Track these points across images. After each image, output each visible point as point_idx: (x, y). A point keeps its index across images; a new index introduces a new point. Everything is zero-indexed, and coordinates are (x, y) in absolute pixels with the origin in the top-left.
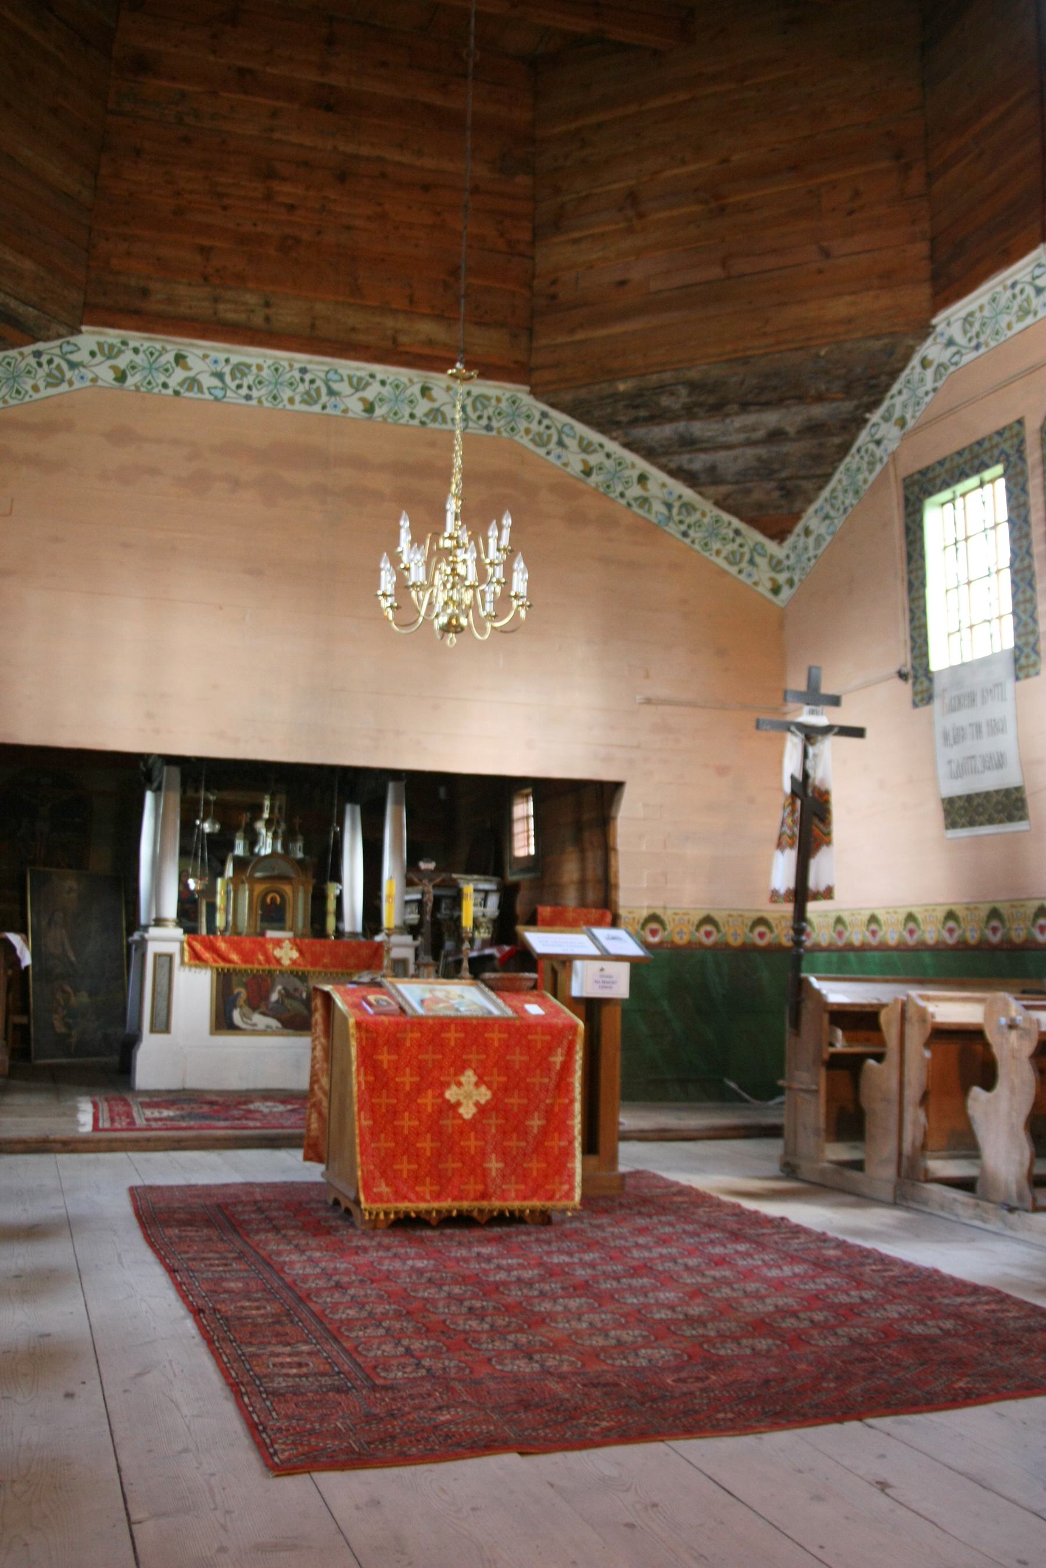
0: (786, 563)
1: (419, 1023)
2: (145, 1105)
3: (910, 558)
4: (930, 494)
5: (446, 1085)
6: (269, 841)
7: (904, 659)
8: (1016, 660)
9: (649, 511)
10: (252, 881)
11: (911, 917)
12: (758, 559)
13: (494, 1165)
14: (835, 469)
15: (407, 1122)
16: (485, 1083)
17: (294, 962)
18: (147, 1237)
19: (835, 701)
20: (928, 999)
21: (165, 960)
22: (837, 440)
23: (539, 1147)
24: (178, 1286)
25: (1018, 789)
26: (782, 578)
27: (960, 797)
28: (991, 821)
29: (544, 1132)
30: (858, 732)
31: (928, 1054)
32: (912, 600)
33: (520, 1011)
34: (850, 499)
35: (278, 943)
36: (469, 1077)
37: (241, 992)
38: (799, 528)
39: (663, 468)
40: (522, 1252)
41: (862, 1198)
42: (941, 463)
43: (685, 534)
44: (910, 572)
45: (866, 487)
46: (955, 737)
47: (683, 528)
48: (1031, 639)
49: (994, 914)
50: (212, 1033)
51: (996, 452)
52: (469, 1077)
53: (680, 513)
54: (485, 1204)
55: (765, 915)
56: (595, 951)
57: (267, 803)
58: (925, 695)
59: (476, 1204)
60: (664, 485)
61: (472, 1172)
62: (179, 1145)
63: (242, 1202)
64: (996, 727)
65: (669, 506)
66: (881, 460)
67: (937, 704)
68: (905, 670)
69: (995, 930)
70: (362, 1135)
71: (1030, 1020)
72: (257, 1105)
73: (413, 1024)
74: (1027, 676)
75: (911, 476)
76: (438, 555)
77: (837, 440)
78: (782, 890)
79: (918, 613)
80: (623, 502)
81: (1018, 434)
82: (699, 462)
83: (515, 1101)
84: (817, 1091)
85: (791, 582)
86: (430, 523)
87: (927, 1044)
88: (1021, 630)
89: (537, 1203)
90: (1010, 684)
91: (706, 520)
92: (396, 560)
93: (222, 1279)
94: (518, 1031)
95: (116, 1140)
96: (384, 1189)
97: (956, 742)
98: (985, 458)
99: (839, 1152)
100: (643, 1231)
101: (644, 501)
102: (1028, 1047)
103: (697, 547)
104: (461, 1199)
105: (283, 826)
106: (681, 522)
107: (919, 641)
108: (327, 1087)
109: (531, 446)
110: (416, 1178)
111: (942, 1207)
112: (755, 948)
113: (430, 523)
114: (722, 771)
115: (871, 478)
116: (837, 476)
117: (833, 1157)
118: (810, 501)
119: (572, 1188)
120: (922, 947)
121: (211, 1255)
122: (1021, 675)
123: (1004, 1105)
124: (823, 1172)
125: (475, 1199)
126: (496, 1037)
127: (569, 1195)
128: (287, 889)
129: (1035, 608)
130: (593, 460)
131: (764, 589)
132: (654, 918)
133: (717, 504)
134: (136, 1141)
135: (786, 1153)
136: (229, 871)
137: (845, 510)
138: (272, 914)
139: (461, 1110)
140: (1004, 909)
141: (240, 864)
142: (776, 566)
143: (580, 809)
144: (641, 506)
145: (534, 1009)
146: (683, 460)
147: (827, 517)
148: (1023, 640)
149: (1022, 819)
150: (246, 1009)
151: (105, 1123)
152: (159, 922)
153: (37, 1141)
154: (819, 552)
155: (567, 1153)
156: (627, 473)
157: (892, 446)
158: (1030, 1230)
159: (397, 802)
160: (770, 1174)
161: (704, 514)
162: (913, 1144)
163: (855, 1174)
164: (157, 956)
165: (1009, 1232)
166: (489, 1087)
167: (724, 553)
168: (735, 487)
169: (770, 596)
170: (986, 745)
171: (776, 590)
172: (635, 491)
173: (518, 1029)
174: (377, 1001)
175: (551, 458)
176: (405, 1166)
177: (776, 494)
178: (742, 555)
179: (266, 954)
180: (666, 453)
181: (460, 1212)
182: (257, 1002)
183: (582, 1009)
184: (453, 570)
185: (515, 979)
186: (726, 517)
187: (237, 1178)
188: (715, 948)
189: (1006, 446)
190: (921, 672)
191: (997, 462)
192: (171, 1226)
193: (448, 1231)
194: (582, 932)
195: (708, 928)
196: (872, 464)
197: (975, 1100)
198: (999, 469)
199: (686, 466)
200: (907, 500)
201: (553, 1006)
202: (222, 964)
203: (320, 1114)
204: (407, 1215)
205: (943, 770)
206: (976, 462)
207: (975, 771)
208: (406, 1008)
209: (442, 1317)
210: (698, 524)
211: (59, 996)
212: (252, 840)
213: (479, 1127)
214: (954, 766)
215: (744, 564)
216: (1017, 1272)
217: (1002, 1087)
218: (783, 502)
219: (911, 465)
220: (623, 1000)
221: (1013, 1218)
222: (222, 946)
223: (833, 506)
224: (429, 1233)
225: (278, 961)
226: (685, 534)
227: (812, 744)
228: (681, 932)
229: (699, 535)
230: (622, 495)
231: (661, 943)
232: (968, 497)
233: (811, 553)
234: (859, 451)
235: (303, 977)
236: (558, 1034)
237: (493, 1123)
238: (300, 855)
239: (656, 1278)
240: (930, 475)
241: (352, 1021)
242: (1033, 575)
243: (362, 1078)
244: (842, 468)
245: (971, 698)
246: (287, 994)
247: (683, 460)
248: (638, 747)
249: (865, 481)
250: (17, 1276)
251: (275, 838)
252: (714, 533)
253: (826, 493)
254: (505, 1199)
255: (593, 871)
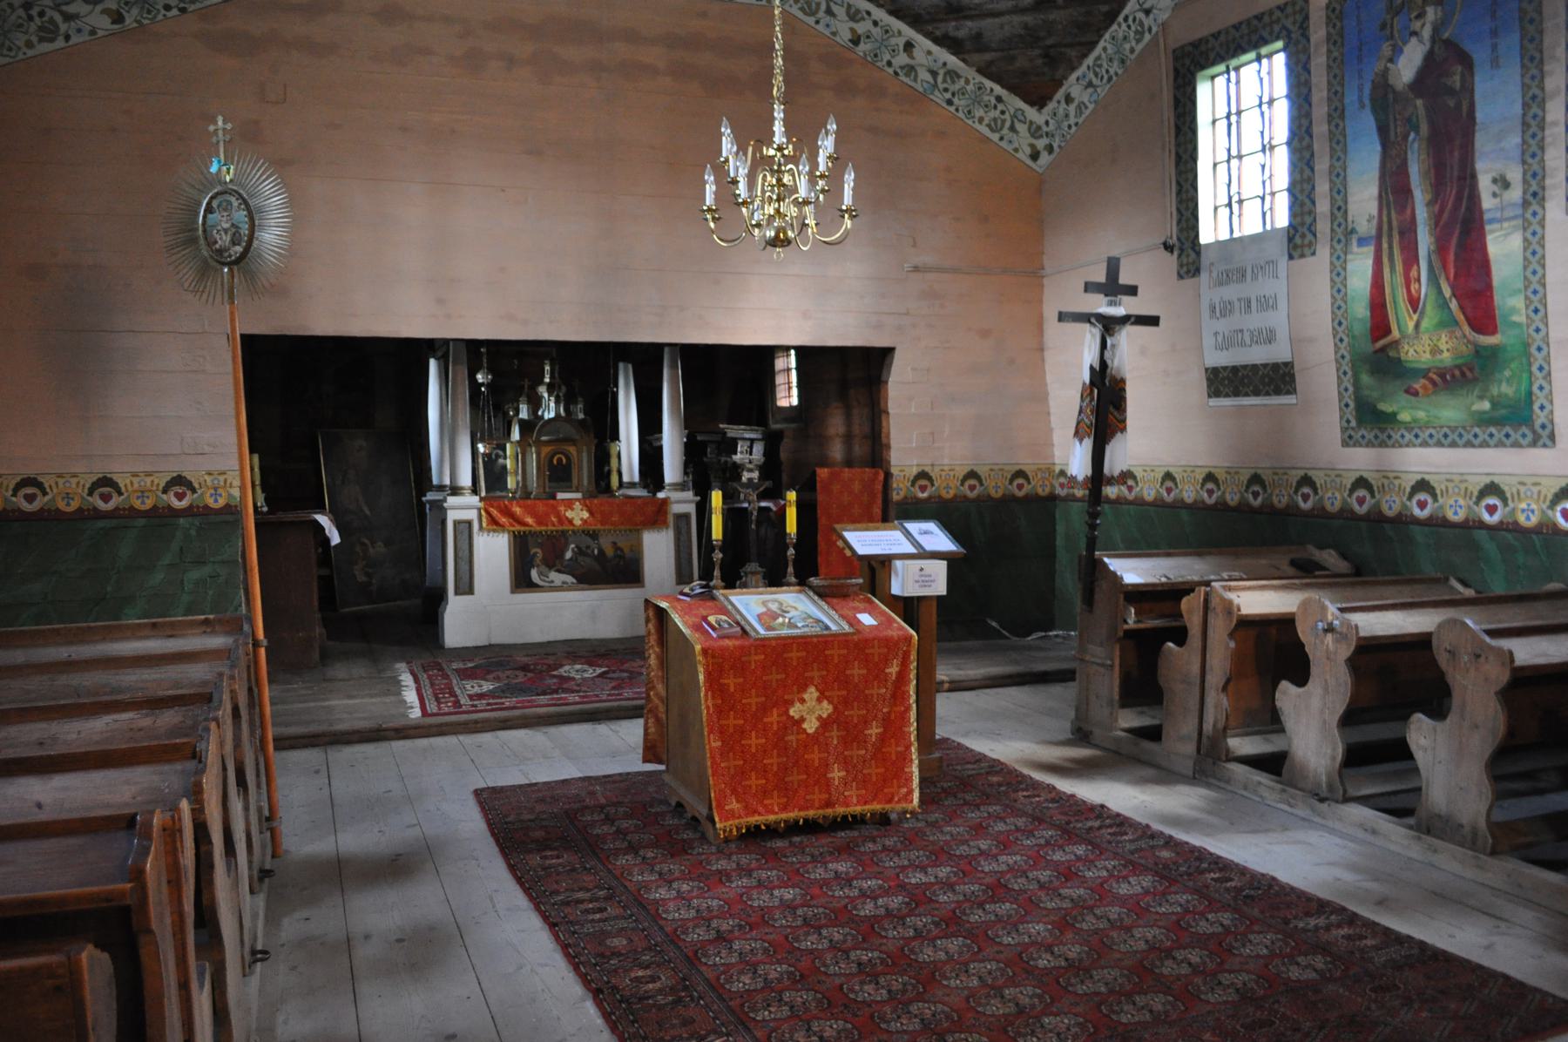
0: (1045, 129)
1: (763, 643)
2: (467, 674)
3: (1178, 129)
4: (1203, 68)
5: (792, 703)
6: (552, 405)
7: (1171, 231)
8: (1290, 240)
9: (915, 80)
10: (538, 443)
11: (1168, 476)
12: (1018, 126)
13: (837, 774)
14: (1101, 36)
15: (754, 741)
16: (827, 698)
17: (585, 522)
18: (512, 869)
19: (1132, 291)
20: (1230, 589)
21: (464, 527)
22: (1105, 8)
23: (879, 754)
24: (564, 947)
25: (1286, 364)
26: (1041, 144)
27: (1225, 368)
28: (1257, 393)
29: (882, 738)
30: (1153, 321)
31: (1232, 644)
32: (1179, 173)
33: (853, 622)
34: (1115, 68)
35: (569, 504)
36: (811, 694)
37: (538, 553)
38: (1060, 95)
39: (928, 35)
40: (876, 869)
41: (1165, 775)
42: (1216, 36)
43: (950, 102)
44: (1178, 145)
45: (1133, 57)
46: (1225, 310)
47: (948, 96)
48: (1308, 220)
49: (1256, 479)
50: (513, 592)
51: (1277, 28)
52: (811, 694)
53: (944, 81)
54: (829, 811)
55: (1023, 468)
56: (912, 550)
57: (547, 368)
58: (1192, 268)
59: (821, 812)
60: (929, 53)
61: (817, 783)
62: (506, 725)
63: (587, 807)
64: (1267, 304)
65: (934, 74)
66: (1150, 30)
67: (1204, 276)
68: (1171, 242)
69: (1256, 495)
70: (712, 757)
71: (1348, 624)
72: (567, 670)
73: (756, 647)
74: (1302, 256)
75: (1182, 47)
76: (760, 163)
77: (1105, 8)
78: (1080, 478)
79: (1187, 186)
80: (890, 70)
81: (1302, 10)
82: (964, 30)
83: (855, 713)
84: (1112, 666)
85: (1050, 149)
86: (754, 134)
87: (1231, 635)
88: (1298, 209)
89: (877, 807)
90: (1283, 262)
91: (970, 88)
92: (720, 170)
93: (604, 934)
94: (857, 645)
95: (446, 724)
96: (734, 805)
97: (1223, 315)
98: (1265, 34)
99: (1129, 719)
100: (979, 829)
101: (910, 70)
102: (1345, 651)
103: (961, 114)
104: (807, 809)
105: (564, 389)
106: (946, 90)
107: (1188, 214)
108: (663, 693)
109: (800, 15)
110: (765, 793)
111: (1245, 788)
112: (1014, 499)
113: (754, 134)
114: (985, 334)
115: (1139, 48)
116: (1102, 44)
117: (1126, 725)
118: (1073, 69)
119: (911, 792)
120: (1179, 505)
121: (580, 895)
122: (1295, 254)
123: (1316, 703)
124: (1118, 740)
125: (821, 808)
126: (835, 653)
127: (908, 797)
128: (572, 450)
129: (1313, 188)
130: (861, 28)
131: (1024, 155)
132: (923, 475)
133: (979, 71)
134: (466, 723)
135: (1077, 718)
136: (516, 435)
137: (1110, 79)
138: (559, 475)
139: (805, 726)
140: (1267, 476)
141: (526, 427)
142: (1035, 132)
143: (850, 376)
144: (907, 75)
145: (866, 619)
146: (950, 27)
147: (1090, 84)
148: (1299, 219)
149: (1288, 393)
150: (543, 568)
151: (432, 707)
152: (455, 490)
153: (371, 731)
154: (1080, 121)
155: (904, 758)
156: (893, 41)
157: (1164, 16)
158: (1340, 820)
159: (673, 366)
160: (1062, 737)
161: (967, 82)
162: (1214, 726)
163: (1148, 745)
164: (457, 523)
165: (1317, 819)
166: (830, 702)
167: (986, 121)
168: (999, 54)
169: (1029, 162)
170: (1255, 321)
171: (1035, 156)
172: (902, 59)
173: (856, 645)
174: (718, 622)
175: (820, 27)
176: (754, 781)
177: (1039, 61)
178: (1004, 121)
179: (558, 515)
180: (933, 20)
181: (806, 820)
182: (553, 561)
183: (901, 605)
184: (779, 180)
185: (842, 586)
186: (988, 84)
187: (568, 771)
188: (978, 500)
189: (1288, 23)
190: (1188, 245)
191: (1277, 39)
192: (530, 852)
193: (797, 839)
194: (895, 528)
195: (972, 482)
196: (1140, 34)
197: (1284, 693)
198: (1280, 44)
199: (952, 33)
200: (1176, 71)
201: (883, 613)
202: (518, 528)
203: (658, 720)
204: (757, 827)
205: (1209, 341)
206: (1254, 38)
207: (1243, 344)
208: (747, 628)
209: (838, 981)
210: (963, 92)
211: (358, 549)
212: (535, 403)
213: (821, 739)
214: (1220, 339)
215: (1005, 131)
216: (1348, 877)
217: (1314, 685)
218: (1046, 69)
219: (1184, 34)
220: (939, 597)
221: (1324, 807)
222: (517, 510)
223: (1096, 75)
224: (779, 844)
225: (570, 522)
226: (950, 102)
227: (1111, 335)
228: (948, 487)
229: (963, 102)
230: (889, 64)
231: (930, 497)
232: (1243, 70)
233: (1072, 121)
234: (1126, 19)
235: (594, 535)
236: (892, 646)
237: (835, 735)
238: (581, 416)
239: (1015, 901)
240: (1203, 48)
241: (698, 648)
242: (1312, 155)
243: (710, 703)
244: (1107, 36)
245: (1242, 274)
246: (580, 552)
247: (950, 27)
248: (907, 314)
249: (1132, 50)
250: (399, 941)
251: (557, 402)
252: (977, 101)
253: (1090, 60)
254: (847, 806)
255: (860, 426)
